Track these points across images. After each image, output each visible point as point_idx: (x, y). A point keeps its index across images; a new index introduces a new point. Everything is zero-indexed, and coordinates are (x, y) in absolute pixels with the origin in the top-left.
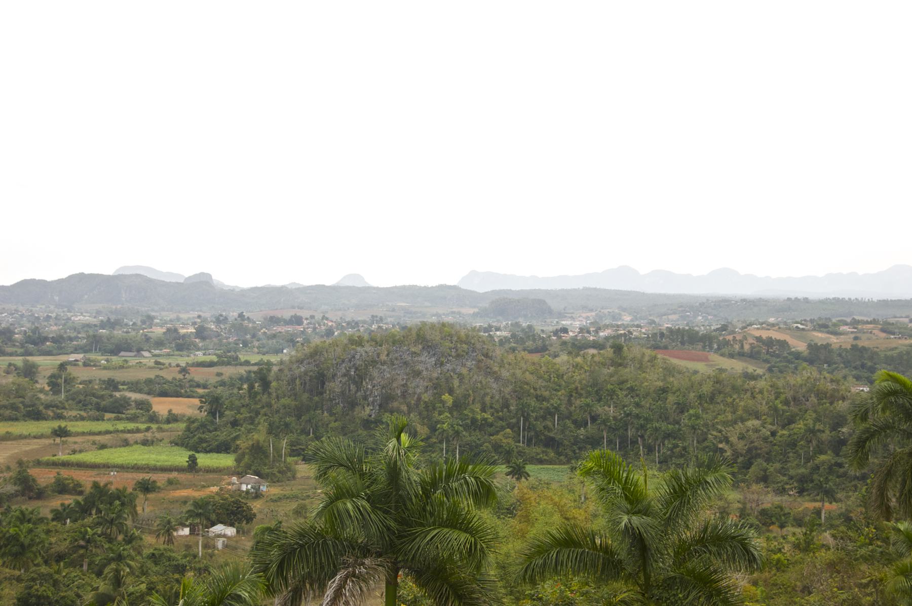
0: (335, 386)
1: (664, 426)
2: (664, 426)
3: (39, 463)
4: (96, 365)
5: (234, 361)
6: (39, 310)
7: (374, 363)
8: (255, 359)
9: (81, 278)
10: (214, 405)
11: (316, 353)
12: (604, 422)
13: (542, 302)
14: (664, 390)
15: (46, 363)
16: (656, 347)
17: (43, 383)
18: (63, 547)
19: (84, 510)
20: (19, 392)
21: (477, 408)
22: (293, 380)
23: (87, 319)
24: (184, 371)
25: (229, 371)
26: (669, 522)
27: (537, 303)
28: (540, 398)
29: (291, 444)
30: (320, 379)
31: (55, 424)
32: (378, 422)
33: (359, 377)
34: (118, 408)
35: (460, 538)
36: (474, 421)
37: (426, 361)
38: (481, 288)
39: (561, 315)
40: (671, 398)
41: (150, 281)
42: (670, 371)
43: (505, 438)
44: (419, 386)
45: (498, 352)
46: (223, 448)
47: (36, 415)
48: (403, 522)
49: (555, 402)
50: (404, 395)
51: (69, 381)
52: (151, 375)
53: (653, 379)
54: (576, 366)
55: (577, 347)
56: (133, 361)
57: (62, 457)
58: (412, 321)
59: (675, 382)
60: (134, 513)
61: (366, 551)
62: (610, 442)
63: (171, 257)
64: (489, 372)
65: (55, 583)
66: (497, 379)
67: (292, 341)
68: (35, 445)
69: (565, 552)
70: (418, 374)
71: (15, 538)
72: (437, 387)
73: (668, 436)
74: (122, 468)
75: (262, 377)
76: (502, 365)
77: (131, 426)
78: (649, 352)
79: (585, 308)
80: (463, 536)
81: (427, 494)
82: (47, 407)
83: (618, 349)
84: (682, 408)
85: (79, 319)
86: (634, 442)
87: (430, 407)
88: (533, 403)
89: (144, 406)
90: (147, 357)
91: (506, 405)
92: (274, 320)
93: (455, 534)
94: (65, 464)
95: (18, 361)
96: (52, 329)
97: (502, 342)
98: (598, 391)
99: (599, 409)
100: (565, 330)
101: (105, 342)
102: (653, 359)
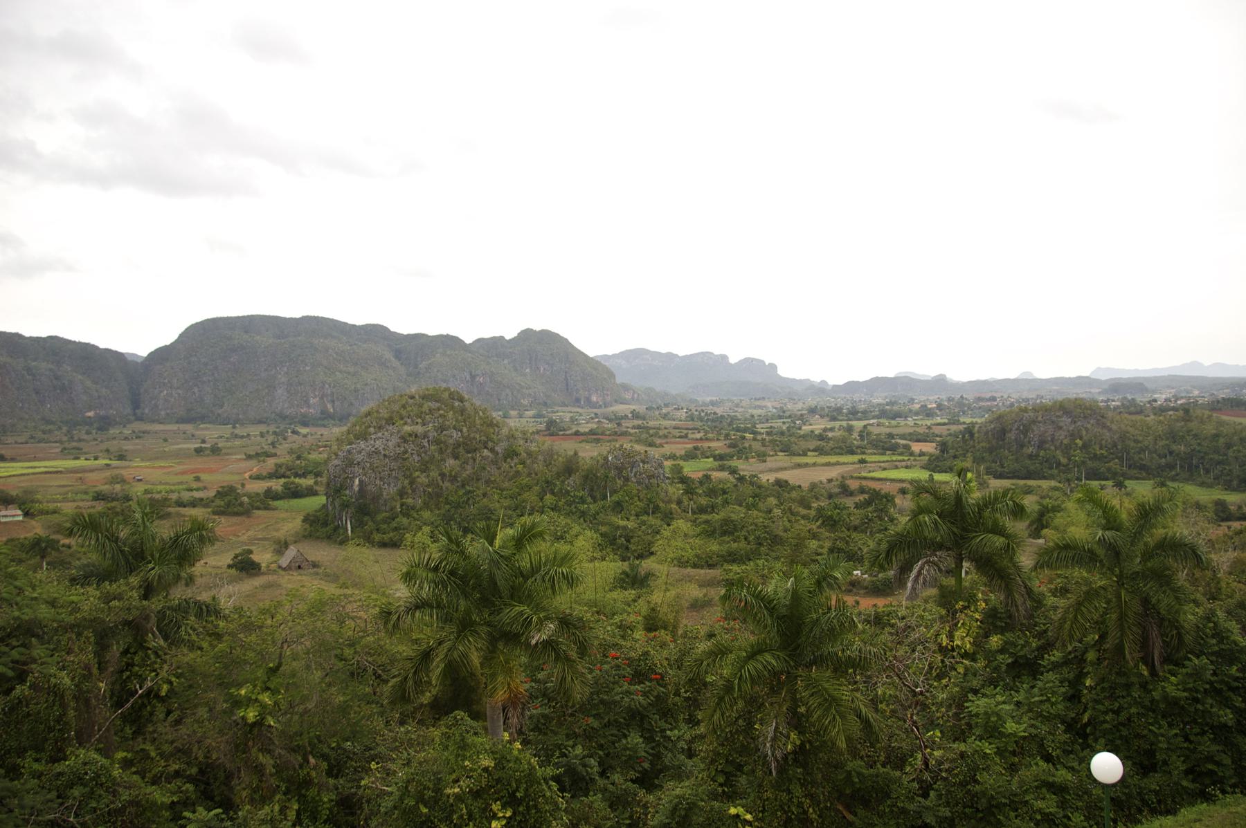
0: (1011, 436)
1: (1216, 457)
2: (1216, 457)
3: (852, 477)
4: (883, 425)
5: (958, 422)
6: (856, 397)
7: (1034, 422)
8: (968, 420)
9: (877, 379)
10: (943, 447)
11: (1000, 417)
12: (1178, 455)
13: (1141, 384)
14: (1217, 436)
15: (858, 424)
16: (1213, 410)
17: (855, 435)
18: (857, 522)
19: (868, 503)
20: (844, 440)
21: (1097, 447)
22: (987, 433)
23: (880, 401)
24: (929, 428)
25: (954, 428)
26: (1138, 535)
27: (1138, 385)
28: (1136, 441)
29: (987, 468)
30: (1002, 432)
31: (860, 457)
32: (1037, 456)
33: (1026, 429)
34: (893, 449)
35: (999, 541)
36: (1095, 455)
37: (1065, 421)
38: (1104, 377)
39: (1154, 392)
40: (1222, 440)
41: (912, 379)
42: (1221, 423)
43: (1115, 465)
44: (1061, 435)
45: (1110, 414)
46: (950, 470)
47: (852, 453)
48: (965, 530)
49: (1146, 443)
50: (1053, 440)
51: (869, 434)
52: (911, 431)
53: (1210, 429)
54: (1160, 422)
55: (1162, 410)
56: (903, 423)
57: (864, 474)
58: (1060, 398)
59: (1225, 430)
60: (895, 506)
61: (941, 546)
62: (1181, 467)
63: (924, 367)
64: (1104, 426)
65: (847, 542)
66: (1110, 430)
67: (989, 410)
68: (851, 467)
69: (1063, 554)
70: (1061, 428)
71: (831, 517)
72: (1072, 435)
73: (1219, 463)
74: (893, 480)
75: (969, 431)
76: (1112, 422)
77: (900, 458)
78: (1207, 413)
79: (1168, 387)
80: (1002, 539)
81: (981, 510)
82: (858, 447)
83: (1187, 411)
84: (1229, 446)
85: (875, 401)
86: (1197, 467)
87: (1068, 447)
88: (1132, 444)
89: (907, 447)
90: (910, 421)
91: (1115, 445)
92: (980, 399)
93: (996, 538)
94: (865, 478)
95: (844, 424)
96: (862, 407)
97: (1116, 408)
98: (1173, 436)
99: (1174, 447)
100: (1155, 401)
101: (889, 413)
102: (1210, 417)
